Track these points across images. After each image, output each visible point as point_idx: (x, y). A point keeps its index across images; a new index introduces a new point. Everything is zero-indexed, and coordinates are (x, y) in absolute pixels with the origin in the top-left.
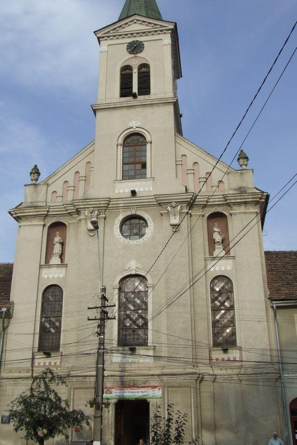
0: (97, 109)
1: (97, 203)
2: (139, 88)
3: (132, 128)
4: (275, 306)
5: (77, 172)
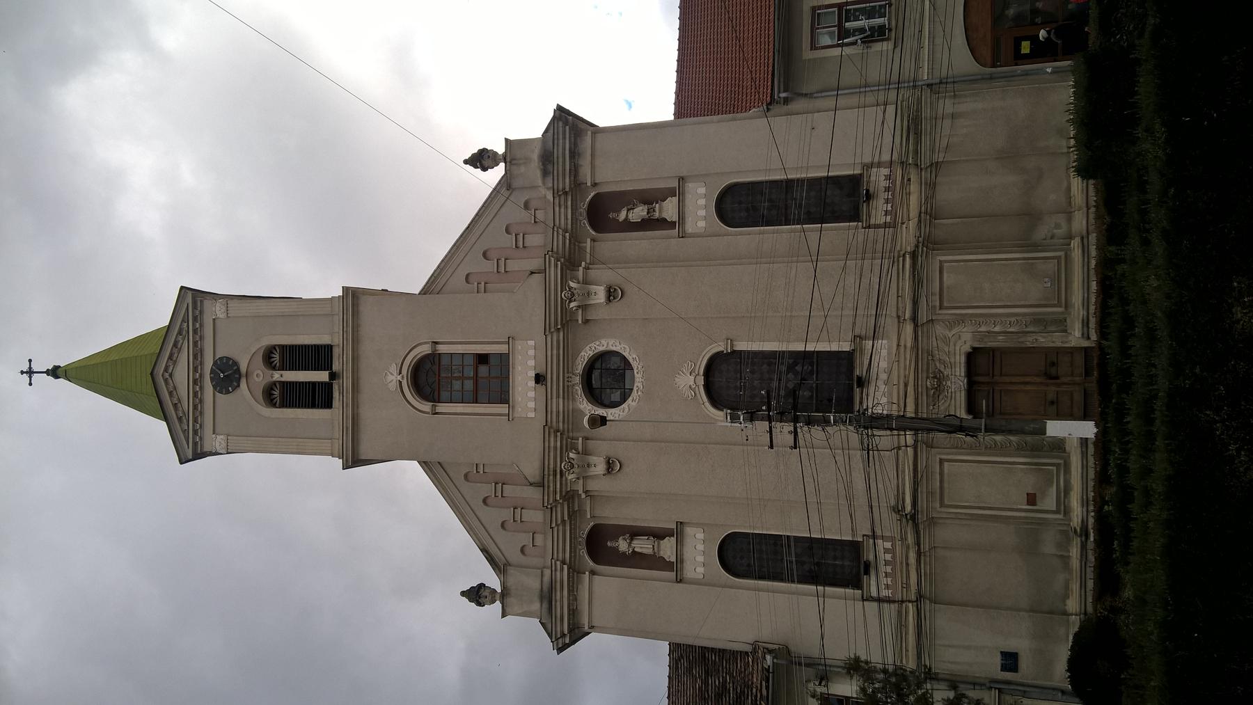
0: (353, 457)
1: (552, 454)
2: (317, 368)
3: (400, 382)
4: (783, 95)
5: (485, 501)
